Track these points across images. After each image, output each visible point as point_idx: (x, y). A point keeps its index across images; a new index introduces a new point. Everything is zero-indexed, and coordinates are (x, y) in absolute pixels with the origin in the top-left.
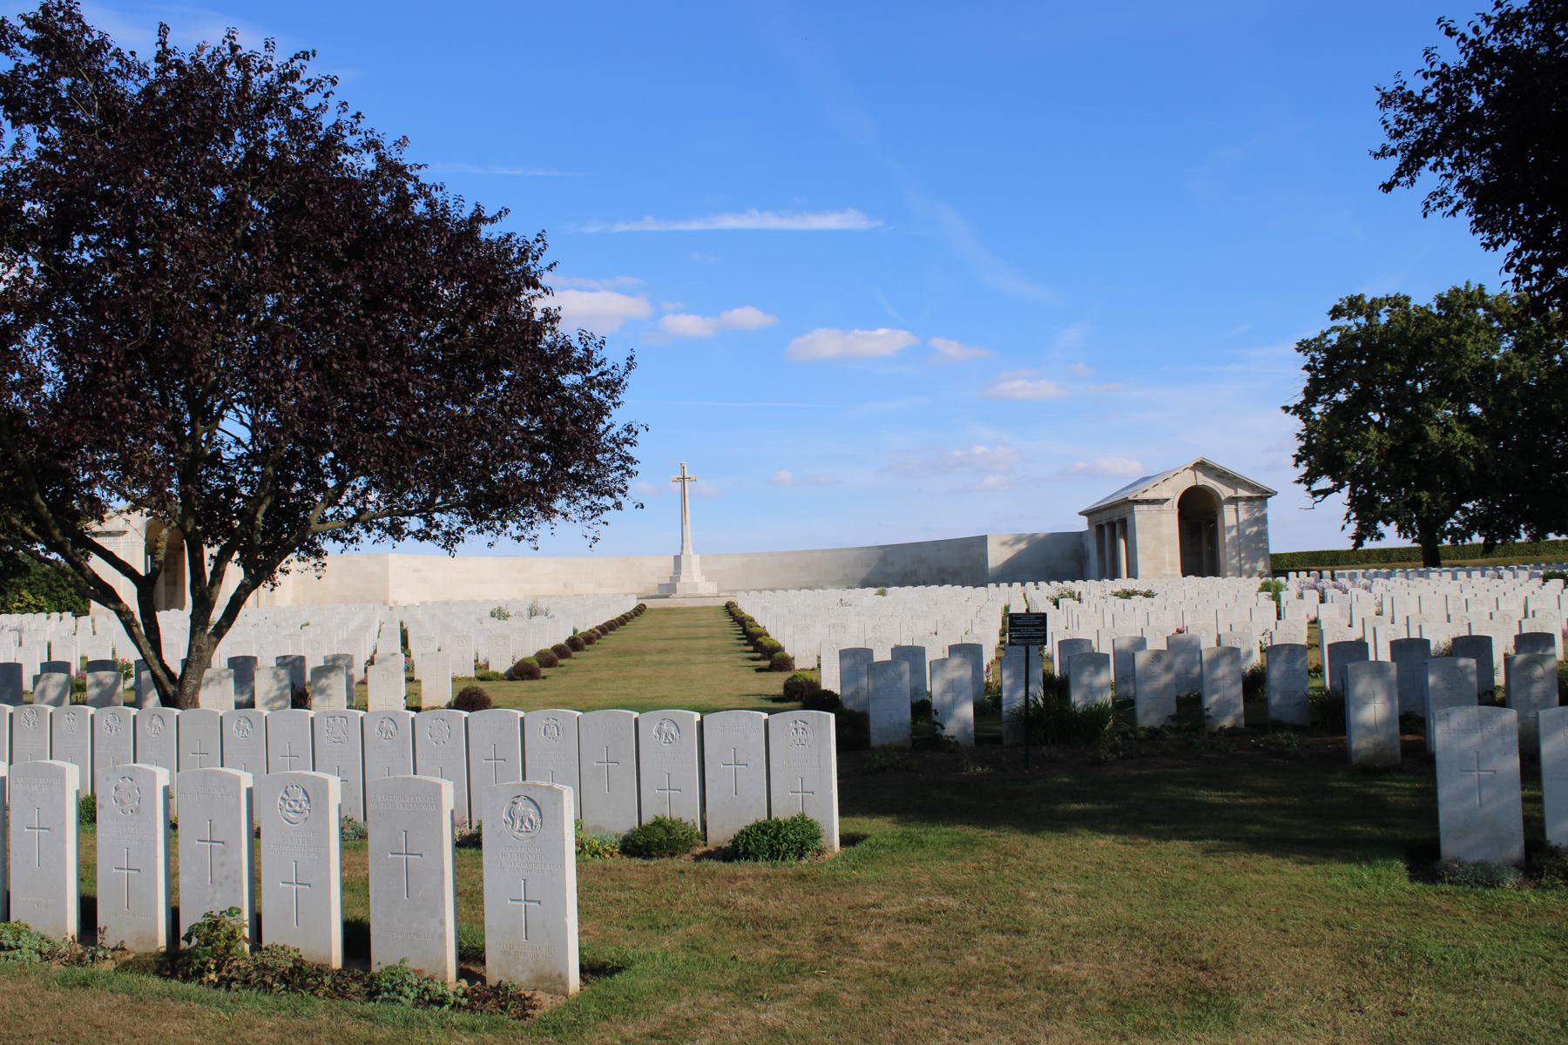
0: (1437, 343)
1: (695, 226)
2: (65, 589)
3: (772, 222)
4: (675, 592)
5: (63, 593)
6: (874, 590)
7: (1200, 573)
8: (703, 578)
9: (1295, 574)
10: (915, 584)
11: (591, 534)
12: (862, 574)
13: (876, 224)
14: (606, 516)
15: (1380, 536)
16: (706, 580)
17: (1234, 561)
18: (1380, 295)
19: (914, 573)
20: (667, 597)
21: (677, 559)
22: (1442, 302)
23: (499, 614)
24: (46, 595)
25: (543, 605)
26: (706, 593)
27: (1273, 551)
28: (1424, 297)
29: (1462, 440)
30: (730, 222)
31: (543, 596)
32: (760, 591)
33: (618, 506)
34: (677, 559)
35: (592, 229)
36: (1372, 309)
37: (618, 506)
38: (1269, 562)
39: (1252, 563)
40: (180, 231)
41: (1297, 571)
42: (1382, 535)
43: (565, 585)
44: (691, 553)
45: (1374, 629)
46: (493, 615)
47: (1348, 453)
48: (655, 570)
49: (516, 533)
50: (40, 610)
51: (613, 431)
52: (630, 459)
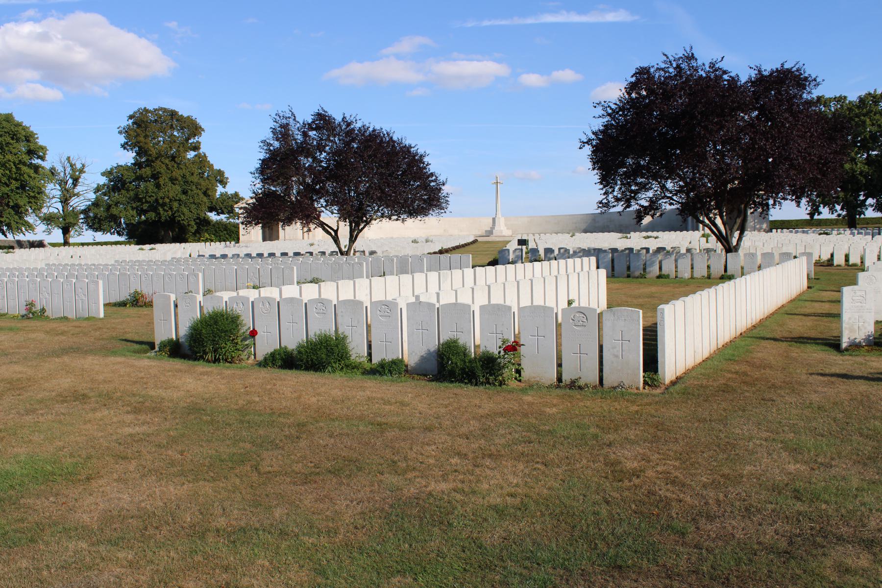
0: (854, 120)
1: (530, 21)
2: (222, 232)
3: (575, 18)
4: (492, 234)
5: (221, 234)
6: (620, 235)
7: (271, 239)
8: (506, 228)
9: (775, 230)
10: (609, 232)
11: (438, 219)
12: (584, 226)
13: (636, 18)
14: (442, 215)
15: (820, 213)
16: (507, 229)
17: (752, 224)
19: (608, 226)
20: (488, 236)
21: (494, 219)
22: (862, 100)
23: (415, 241)
24: (214, 234)
25: (430, 239)
26: (506, 235)
28: (853, 97)
29: (860, 168)
30: (549, 19)
31: (435, 236)
32: (557, 233)
33: (445, 212)
34: (494, 219)
35: (470, 25)
37: (445, 212)
38: (769, 224)
39: (760, 224)
42: (821, 213)
43: (445, 230)
44: (500, 216)
46: (413, 242)
48: (486, 224)
49: (420, 219)
50: (212, 241)
51: (443, 195)
52: (448, 201)
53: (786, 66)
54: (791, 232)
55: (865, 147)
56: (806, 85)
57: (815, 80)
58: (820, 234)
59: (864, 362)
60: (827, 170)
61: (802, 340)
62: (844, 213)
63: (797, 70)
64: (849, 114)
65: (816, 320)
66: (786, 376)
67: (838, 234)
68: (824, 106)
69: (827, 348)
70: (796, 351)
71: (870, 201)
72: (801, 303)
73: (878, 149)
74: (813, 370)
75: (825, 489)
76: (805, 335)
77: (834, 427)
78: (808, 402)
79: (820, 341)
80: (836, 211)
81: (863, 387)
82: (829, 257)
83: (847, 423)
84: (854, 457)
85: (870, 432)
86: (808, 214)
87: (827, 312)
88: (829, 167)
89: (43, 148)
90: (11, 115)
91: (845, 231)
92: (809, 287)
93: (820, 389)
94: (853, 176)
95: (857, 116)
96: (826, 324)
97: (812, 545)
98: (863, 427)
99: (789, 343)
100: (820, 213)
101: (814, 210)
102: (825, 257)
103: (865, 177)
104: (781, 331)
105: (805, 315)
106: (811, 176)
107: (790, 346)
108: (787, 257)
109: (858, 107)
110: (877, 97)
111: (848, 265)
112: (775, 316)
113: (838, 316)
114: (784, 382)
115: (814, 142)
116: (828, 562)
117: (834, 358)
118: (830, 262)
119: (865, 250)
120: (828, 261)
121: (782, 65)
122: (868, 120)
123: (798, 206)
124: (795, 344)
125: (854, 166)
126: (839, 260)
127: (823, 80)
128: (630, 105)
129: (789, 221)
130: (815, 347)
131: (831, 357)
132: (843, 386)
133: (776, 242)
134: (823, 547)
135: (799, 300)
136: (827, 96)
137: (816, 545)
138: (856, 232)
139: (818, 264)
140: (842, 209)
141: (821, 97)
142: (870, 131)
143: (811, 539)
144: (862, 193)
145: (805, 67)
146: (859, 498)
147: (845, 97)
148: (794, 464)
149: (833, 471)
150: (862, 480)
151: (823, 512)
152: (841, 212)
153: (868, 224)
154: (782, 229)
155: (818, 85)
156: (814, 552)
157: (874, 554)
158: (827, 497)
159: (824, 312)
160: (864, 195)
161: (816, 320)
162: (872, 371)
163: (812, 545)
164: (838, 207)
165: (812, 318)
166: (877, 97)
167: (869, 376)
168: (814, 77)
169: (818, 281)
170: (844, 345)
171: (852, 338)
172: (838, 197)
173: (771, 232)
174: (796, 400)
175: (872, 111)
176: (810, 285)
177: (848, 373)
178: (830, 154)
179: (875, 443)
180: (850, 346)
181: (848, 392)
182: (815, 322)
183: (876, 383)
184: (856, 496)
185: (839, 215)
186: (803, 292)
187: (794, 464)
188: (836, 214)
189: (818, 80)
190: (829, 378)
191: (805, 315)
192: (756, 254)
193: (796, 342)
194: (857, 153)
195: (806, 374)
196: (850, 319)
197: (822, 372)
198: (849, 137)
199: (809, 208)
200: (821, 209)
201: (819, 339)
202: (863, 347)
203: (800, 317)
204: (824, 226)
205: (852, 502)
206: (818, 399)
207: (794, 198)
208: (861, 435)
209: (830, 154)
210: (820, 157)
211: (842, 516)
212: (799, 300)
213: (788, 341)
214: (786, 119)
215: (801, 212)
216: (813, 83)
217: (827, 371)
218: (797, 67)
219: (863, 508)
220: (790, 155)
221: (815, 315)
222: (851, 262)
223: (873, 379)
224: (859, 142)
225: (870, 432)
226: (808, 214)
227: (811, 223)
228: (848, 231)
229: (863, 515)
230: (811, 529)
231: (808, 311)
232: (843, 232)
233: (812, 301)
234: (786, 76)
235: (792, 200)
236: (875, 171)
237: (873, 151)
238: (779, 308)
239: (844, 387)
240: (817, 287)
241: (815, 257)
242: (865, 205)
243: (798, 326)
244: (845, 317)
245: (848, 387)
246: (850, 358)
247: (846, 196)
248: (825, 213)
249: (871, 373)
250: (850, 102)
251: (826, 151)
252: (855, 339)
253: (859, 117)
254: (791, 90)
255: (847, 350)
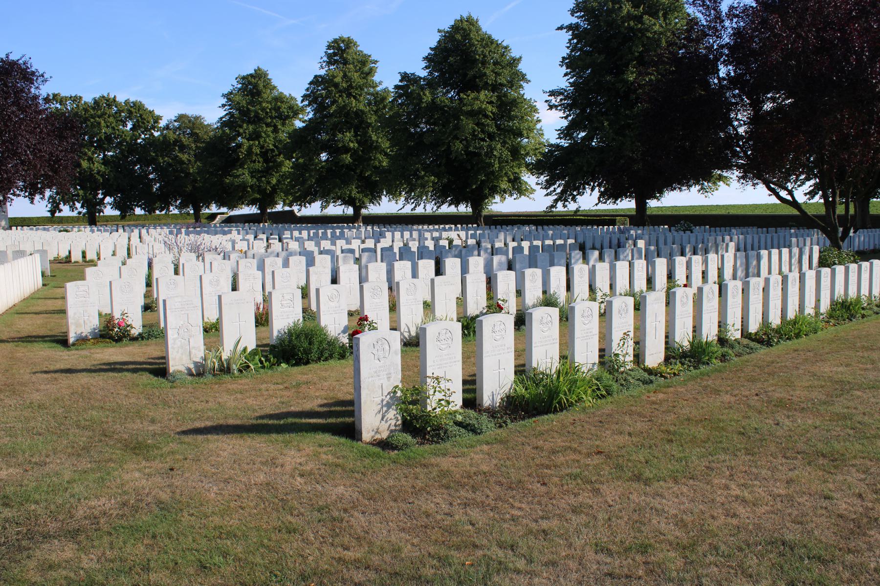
0: (89, 120)
15: (60, 211)
18: (68, 95)
22: (96, 102)
27: (10, 216)
28: (88, 98)
36: (62, 101)
40: (439, 517)
41: (17, 227)
45: (211, 263)
47: (685, 5)
53: (12, 57)
54: (32, 229)
55: (101, 148)
56: (33, 80)
57: (43, 76)
58: (60, 231)
59: (89, 354)
60: (59, 167)
61: (30, 339)
62: (85, 211)
63: (25, 63)
64: (85, 114)
65: (47, 318)
66: (8, 378)
67: (79, 231)
68: (61, 104)
69: (54, 345)
70: (23, 351)
71: (108, 200)
72: (33, 301)
73: (113, 150)
74: (38, 369)
75: (36, 489)
76: (34, 334)
77: (53, 424)
78: (28, 402)
79: (49, 339)
80: (77, 208)
81: (85, 379)
82: (68, 254)
83: (66, 417)
84: (70, 450)
85: (87, 423)
86: (49, 211)
87: (59, 309)
88: (61, 165)
89: (351, 314)
90: (259, 69)
91: (85, 228)
92: (44, 285)
93: (42, 387)
94: (92, 175)
95: (93, 117)
96: (57, 321)
97: (17, 550)
98: (81, 418)
99: (15, 343)
100: (60, 211)
101: (54, 207)
102: (63, 254)
103: (102, 176)
104: (8, 332)
105: (36, 313)
106: (43, 173)
107: (16, 346)
108: (20, 254)
109: (94, 108)
110: (110, 101)
111: (86, 262)
112: (4, 316)
113: (63, 312)
114: (5, 384)
115: (44, 139)
116: (32, 564)
117: (61, 354)
118: (68, 260)
119: (115, 246)
120: (67, 258)
121: (7, 56)
122: (103, 122)
123: (32, 202)
124: (22, 344)
125: (92, 165)
126: (76, 257)
127: (51, 77)
128: (419, 127)
129: (30, 219)
130: (42, 345)
131: (58, 353)
132: (65, 381)
133: (13, 239)
134: (30, 548)
135: (32, 298)
136: (63, 94)
137: (20, 549)
138: (95, 229)
139: (57, 261)
140: (82, 207)
141: (57, 95)
142: (105, 133)
143: (16, 544)
144: (100, 192)
145: (31, 61)
146: (69, 490)
147: (81, 98)
148: (7, 469)
149: (47, 469)
150: (75, 471)
151: (32, 513)
152: (81, 210)
153: (107, 221)
154: (22, 226)
155: (46, 81)
156: (19, 557)
157: (79, 543)
158: (37, 497)
159: (56, 309)
160: (102, 194)
161: (47, 318)
162: (95, 363)
163: (17, 550)
164: (78, 205)
165: (43, 315)
166: (110, 101)
167: (93, 368)
168: (41, 72)
169: (54, 278)
170: (71, 340)
171: (79, 332)
172: (78, 195)
173: (11, 229)
174: (15, 401)
175: (106, 113)
176: (46, 283)
177: (72, 367)
178: (61, 151)
179: (91, 433)
180: (77, 340)
181: (70, 387)
182: (45, 320)
183: (97, 374)
184: (67, 489)
185: (80, 213)
186: (38, 290)
187: (7, 469)
188: (76, 212)
189: (46, 76)
190: (53, 375)
191: (36, 313)
192: (6, 252)
193: (23, 342)
194: (94, 153)
195: (30, 373)
196: (75, 314)
197: (46, 369)
198: (86, 137)
199: (50, 205)
200: (62, 206)
201: (47, 336)
202: (89, 340)
203: (31, 315)
204: (65, 223)
205: (62, 496)
206: (38, 398)
207: (27, 194)
208: (78, 427)
209: (61, 151)
210: (51, 154)
211: (51, 512)
212: (32, 298)
213: (16, 341)
214: (13, 112)
215: (40, 207)
216: (40, 79)
217: (52, 368)
218: (23, 59)
219: (72, 500)
220: (17, 149)
221: (46, 312)
222: (88, 258)
223: (95, 371)
224: (96, 142)
225: (87, 423)
226: (49, 211)
227: (52, 220)
228: (88, 228)
229: (72, 506)
230: (18, 534)
231: (40, 309)
232: (83, 229)
233: (45, 298)
234: (12, 67)
235: (25, 197)
236: (111, 171)
237: (108, 152)
238: (10, 308)
239: (67, 382)
240: (52, 284)
241: (51, 257)
242: (104, 203)
243: (28, 325)
244: (71, 312)
245: (71, 382)
246: (76, 352)
247: (85, 194)
248: (66, 211)
249: (94, 365)
250: (85, 103)
251: (57, 148)
252: (82, 333)
253: (94, 118)
254: (18, 83)
255: (74, 345)
